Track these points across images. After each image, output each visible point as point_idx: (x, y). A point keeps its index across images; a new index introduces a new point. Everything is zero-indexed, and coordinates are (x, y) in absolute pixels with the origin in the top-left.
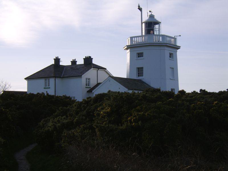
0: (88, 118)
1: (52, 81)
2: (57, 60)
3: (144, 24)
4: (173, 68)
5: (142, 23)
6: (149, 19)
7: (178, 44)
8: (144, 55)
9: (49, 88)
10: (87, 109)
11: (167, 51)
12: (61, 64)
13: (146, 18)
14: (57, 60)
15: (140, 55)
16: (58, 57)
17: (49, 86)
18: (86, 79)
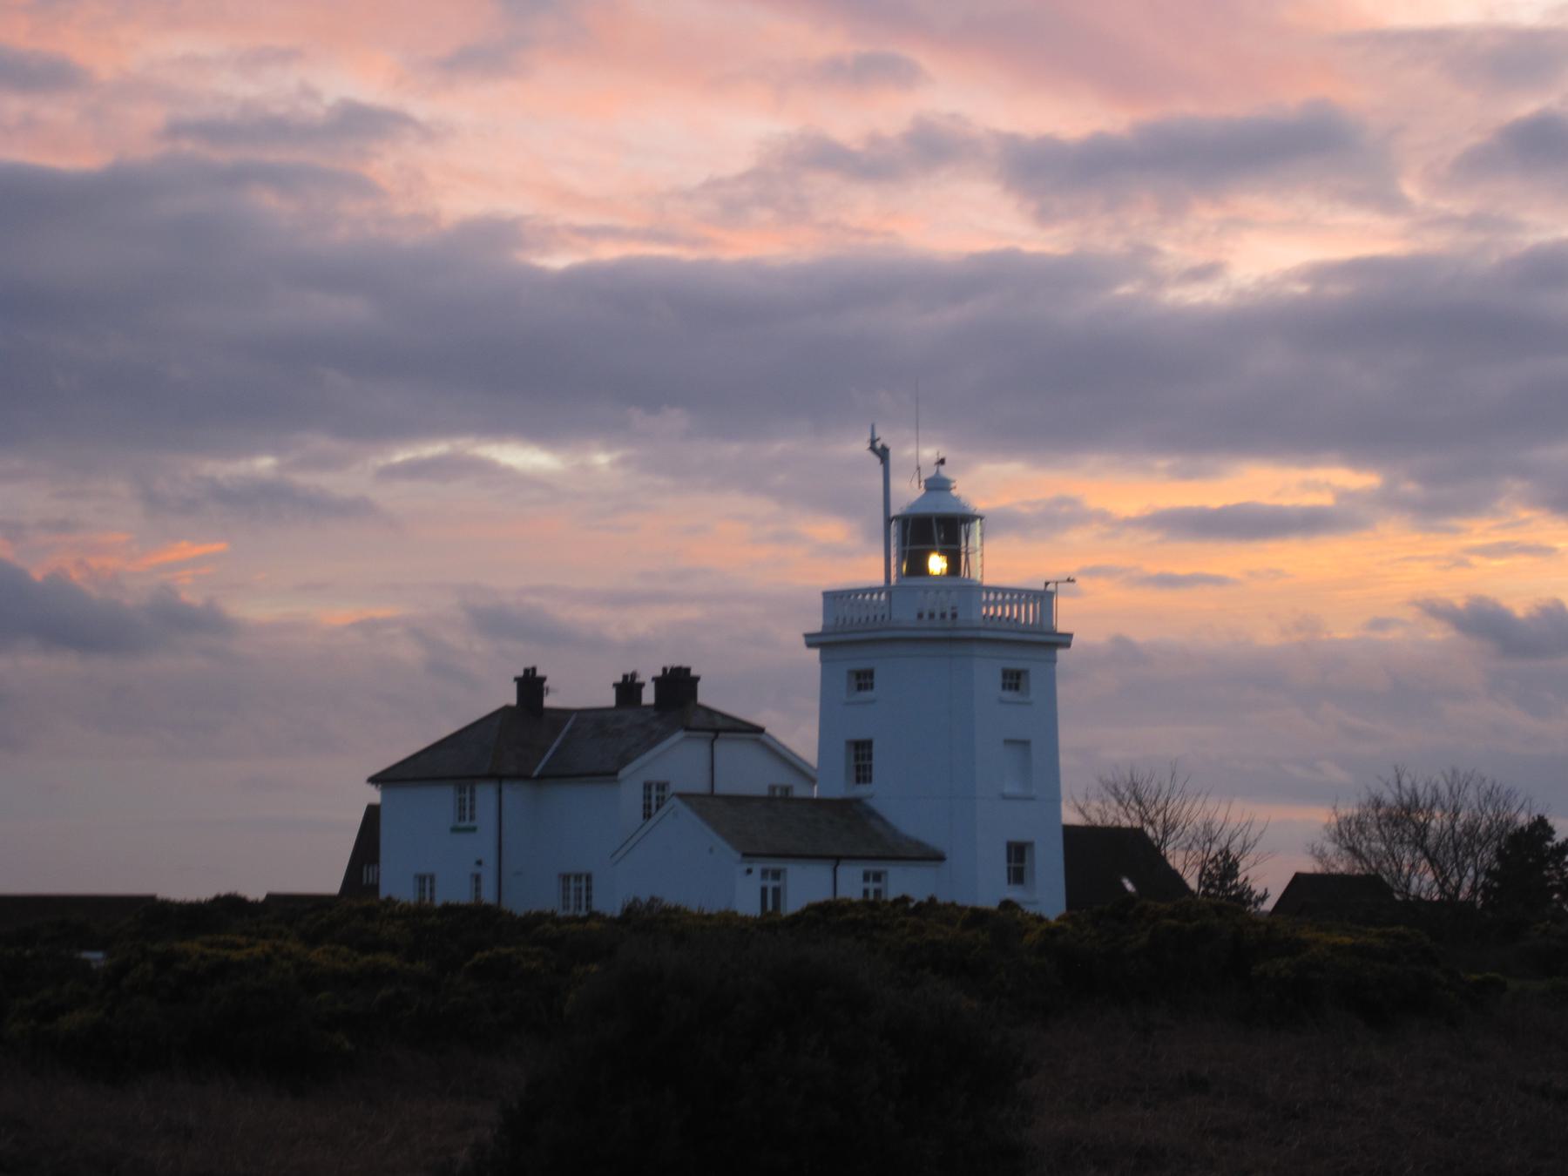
0: (1479, 905)
1: (485, 795)
2: (531, 685)
3: (894, 528)
4: (1025, 743)
5: (888, 520)
6: (923, 497)
7: (1062, 627)
8: (877, 680)
9: (474, 829)
10: (487, 953)
11: (986, 670)
12: (549, 701)
13: (908, 493)
14: (531, 685)
15: (863, 680)
16: (534, 670)
17: (472, 818)
18: (647, 786)
